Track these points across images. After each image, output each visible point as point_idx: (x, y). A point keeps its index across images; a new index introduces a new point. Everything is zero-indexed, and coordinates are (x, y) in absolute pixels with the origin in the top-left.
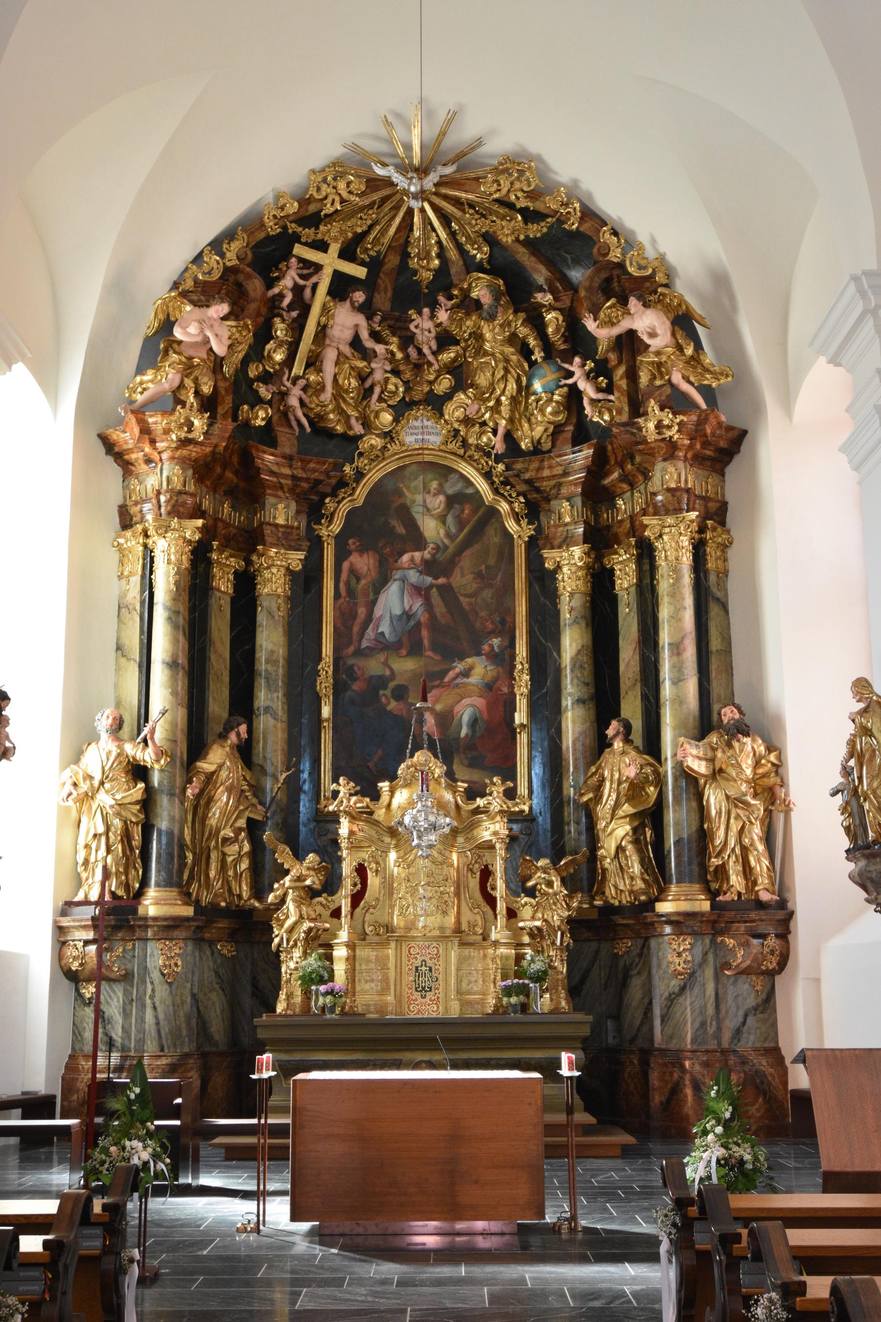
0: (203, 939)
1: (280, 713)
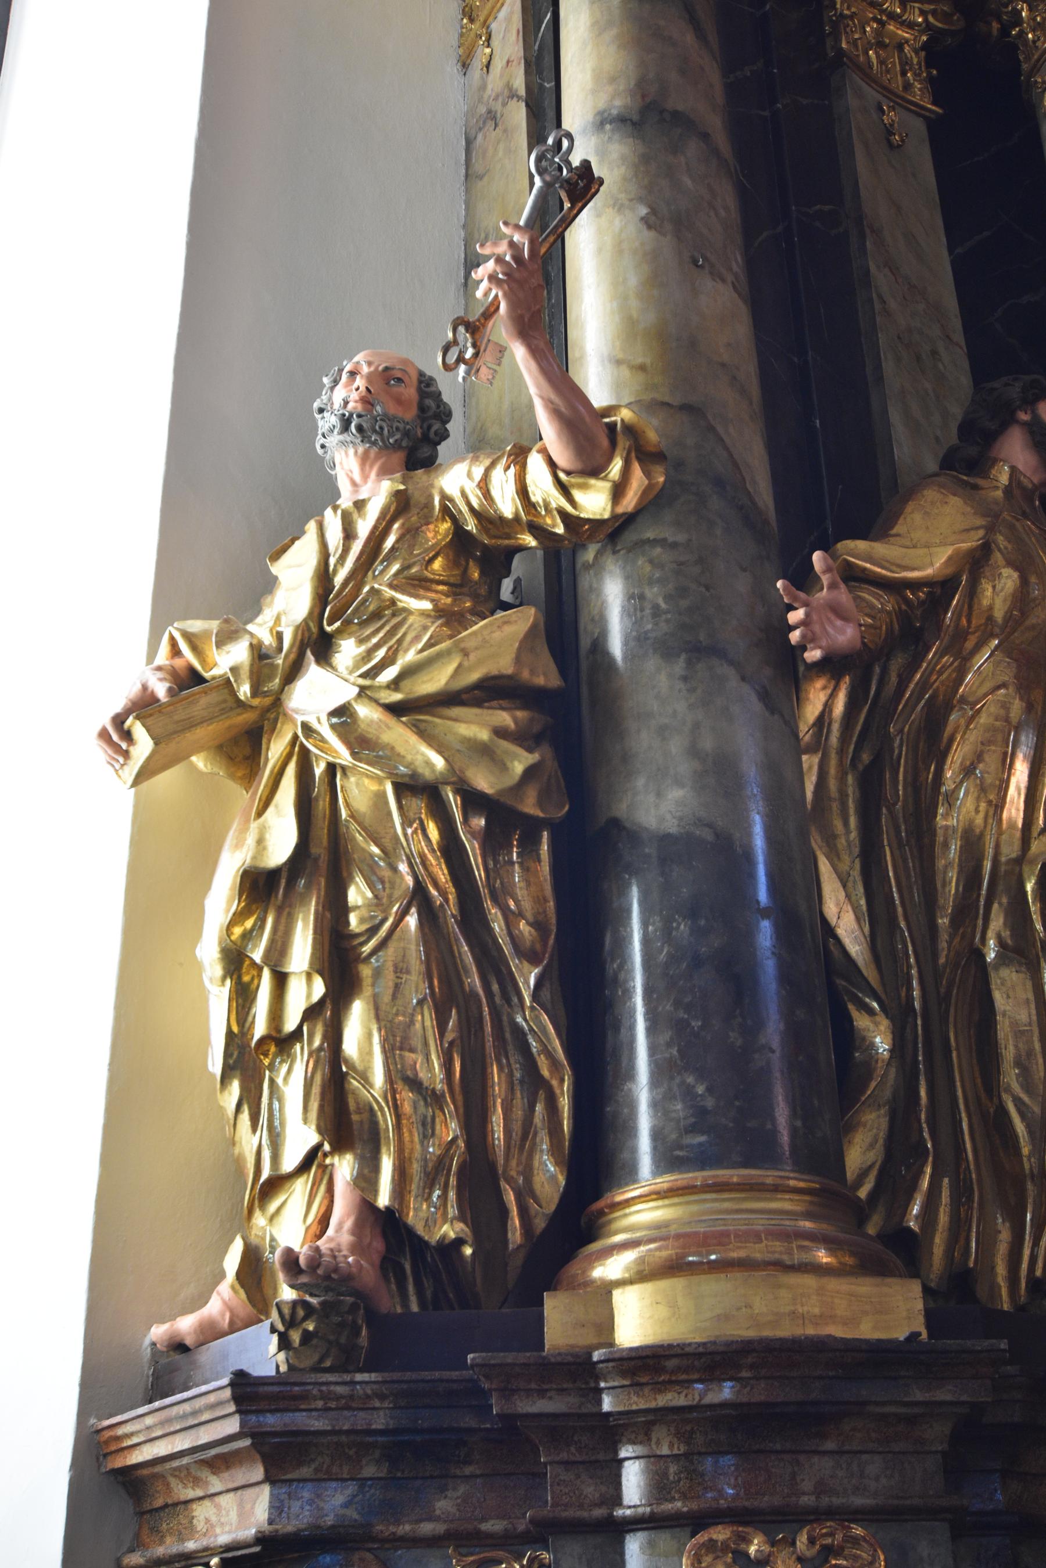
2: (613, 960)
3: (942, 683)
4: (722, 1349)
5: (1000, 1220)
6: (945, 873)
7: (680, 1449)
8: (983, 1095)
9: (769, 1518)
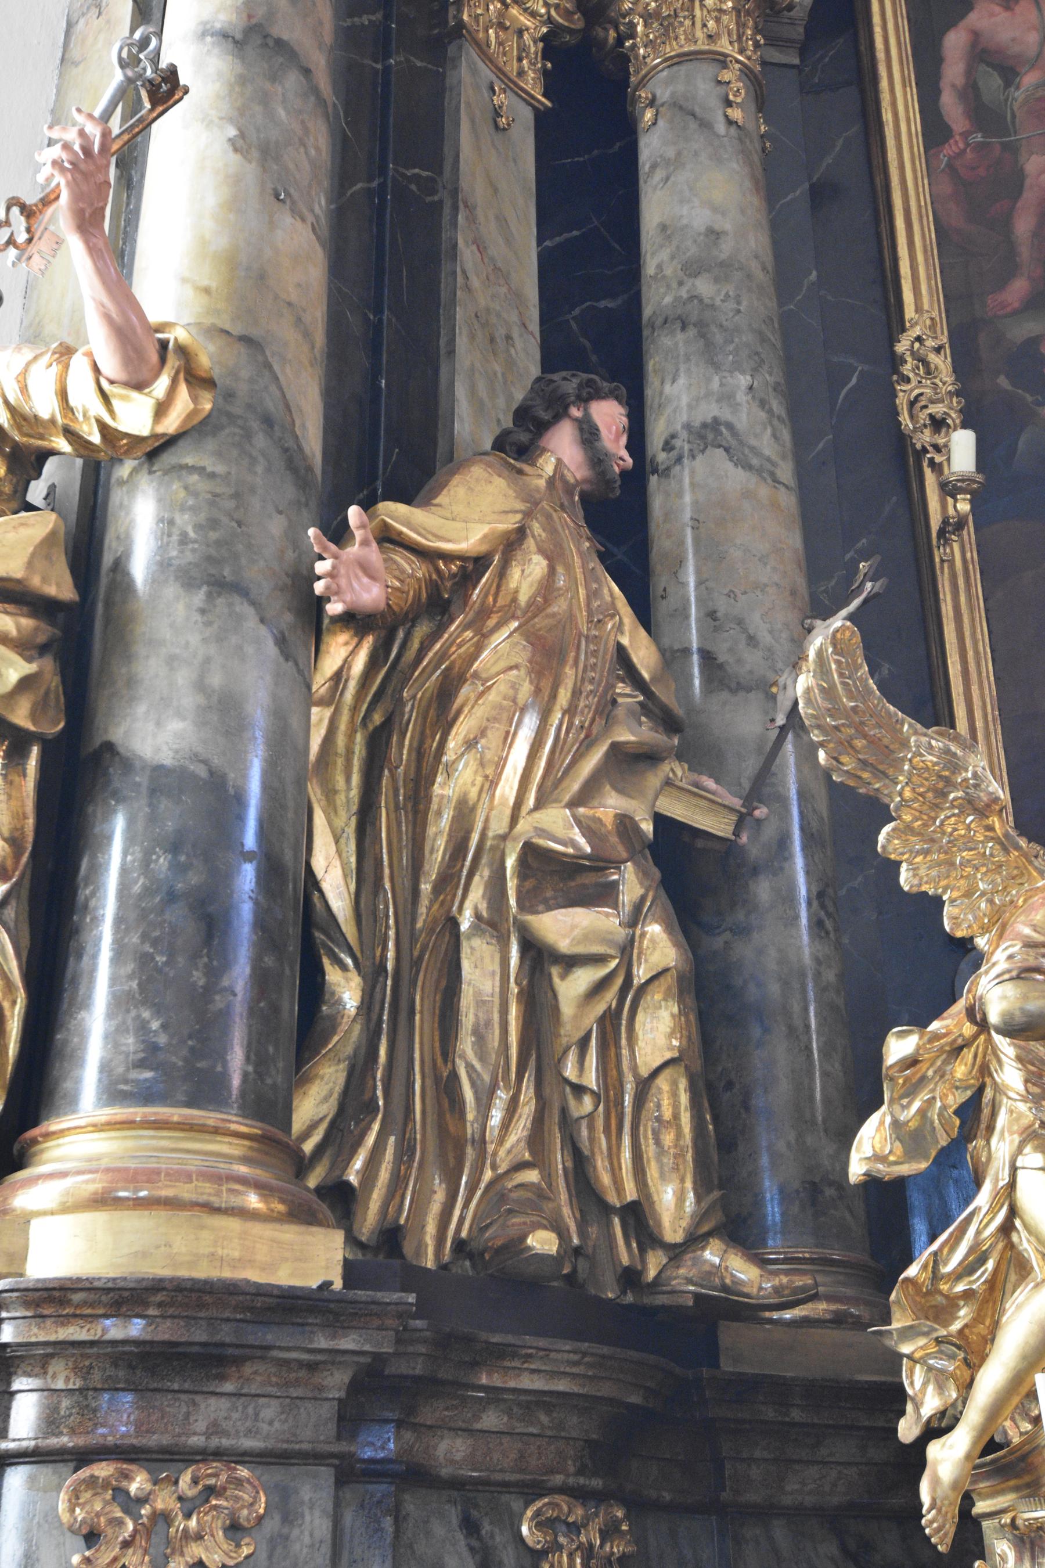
0: (413, 1475)
1: (766, 445)
2: (86, 885)
3: (460, 656)
4: (132, 1285)
5: (437, 1181)
6: (435, 840)
7: (76, 1383)
8: (440, 1061)
9: (154, 1456)
